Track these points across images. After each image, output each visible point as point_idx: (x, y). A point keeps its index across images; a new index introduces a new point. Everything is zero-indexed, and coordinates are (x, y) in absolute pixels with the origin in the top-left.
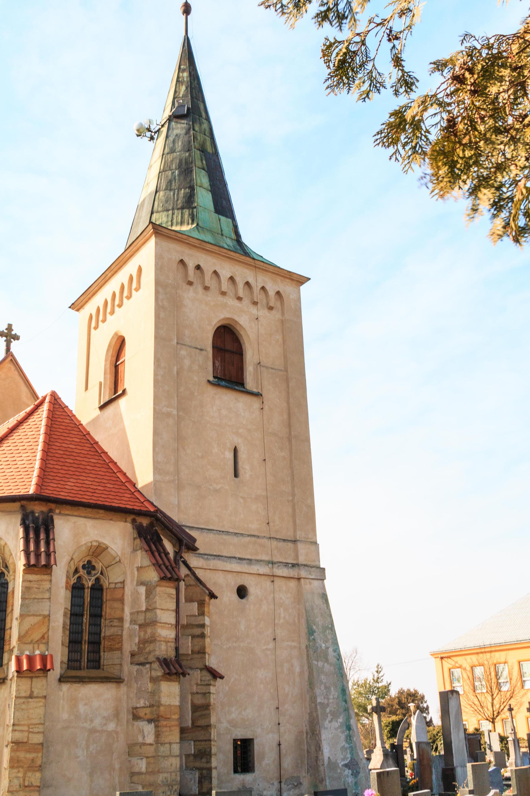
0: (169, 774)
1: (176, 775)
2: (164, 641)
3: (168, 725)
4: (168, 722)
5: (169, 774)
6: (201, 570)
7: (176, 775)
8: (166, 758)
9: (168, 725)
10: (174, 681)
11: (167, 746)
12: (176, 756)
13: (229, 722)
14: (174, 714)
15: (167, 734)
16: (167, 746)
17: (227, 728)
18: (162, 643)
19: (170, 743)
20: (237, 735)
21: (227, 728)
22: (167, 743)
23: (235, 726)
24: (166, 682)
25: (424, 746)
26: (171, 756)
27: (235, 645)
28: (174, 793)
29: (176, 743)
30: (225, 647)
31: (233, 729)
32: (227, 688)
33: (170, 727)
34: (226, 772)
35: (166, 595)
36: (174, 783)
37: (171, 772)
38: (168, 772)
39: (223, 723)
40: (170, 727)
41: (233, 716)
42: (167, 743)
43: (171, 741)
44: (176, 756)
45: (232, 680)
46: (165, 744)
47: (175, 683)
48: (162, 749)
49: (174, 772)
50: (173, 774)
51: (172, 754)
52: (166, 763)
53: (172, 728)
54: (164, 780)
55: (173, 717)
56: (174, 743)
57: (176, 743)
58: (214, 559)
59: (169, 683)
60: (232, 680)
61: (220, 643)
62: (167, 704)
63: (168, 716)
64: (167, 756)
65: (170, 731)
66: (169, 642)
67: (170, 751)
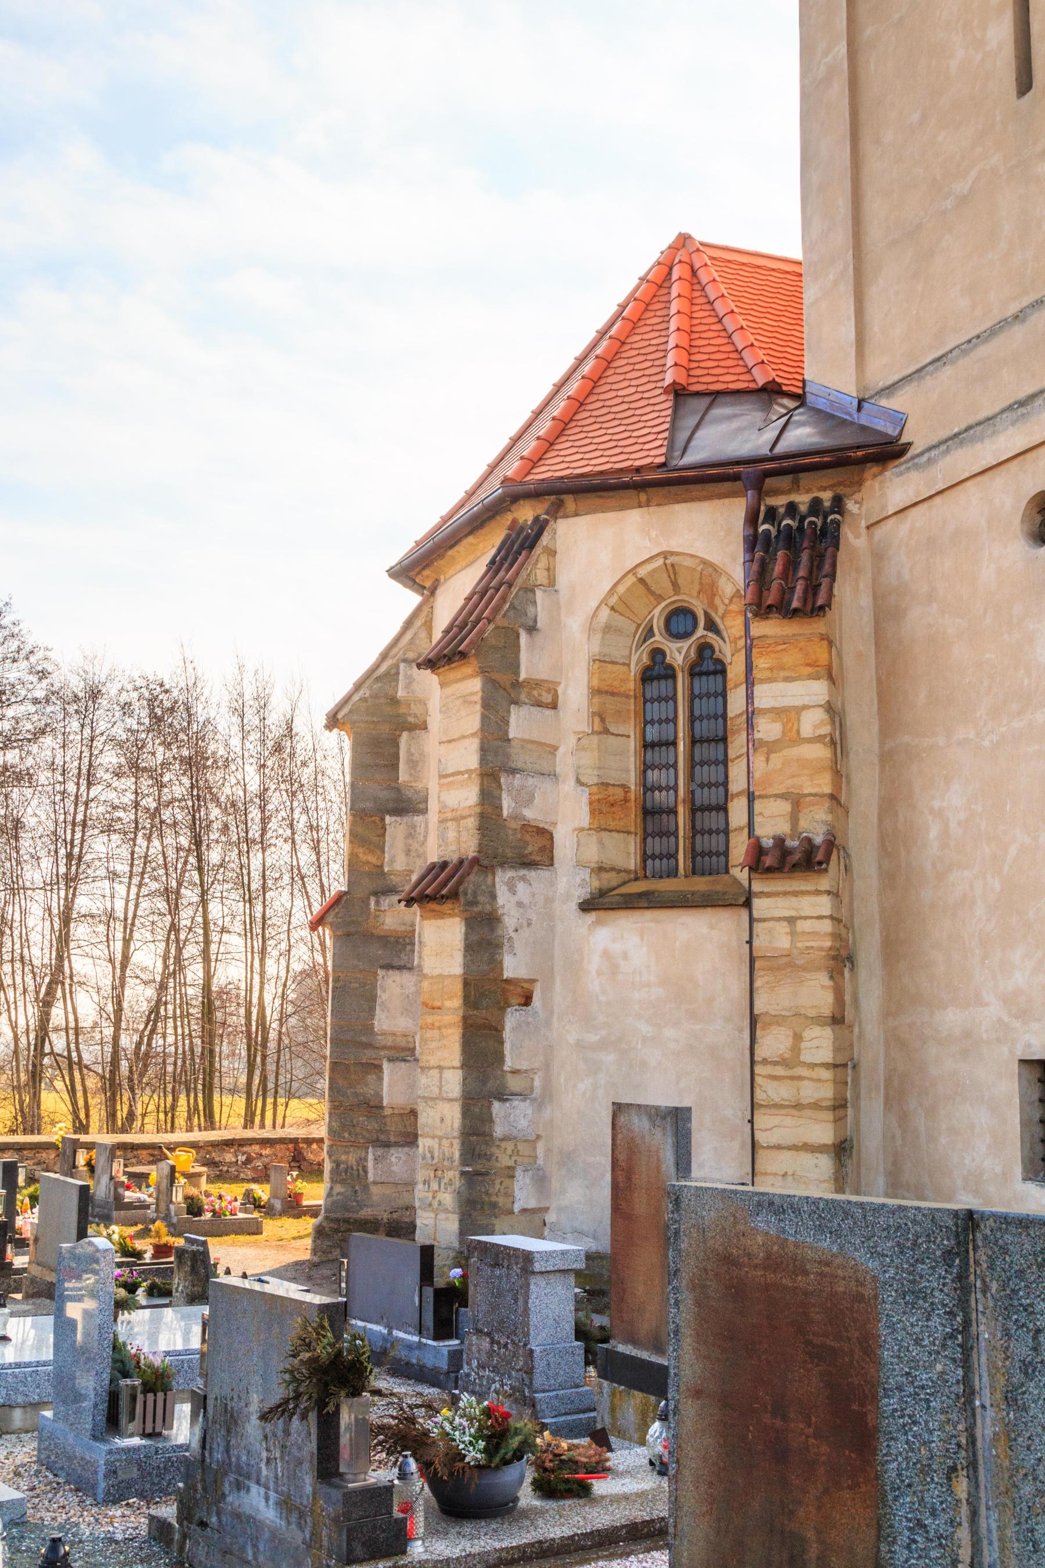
0: (437, 1140)
1: (452, 1145)
2: (451, 820)
3: (437, 1024)
4: (436, 1017)
5: (437, 1140)
6: (915, 510)
7: (452, 1145)
8: (430, 1103)
9: (437, 1024)
10: (451, 916)
11: (434, 1073)
12: (452, 1100)
13: (1008, 1001)
14: (451, 998)
15: (434, 1045)
16: (434, 1073)
17: (1000, 1020)
18: (450, 823)
19: (440, 1068)
20: (1029, 1046)
21: (1000, 1020)
22: (434, 1068)
23: (1024, 1014)
24: (433, 921)
25: (639, 1124)
26: (440, 1098)
27: (1018, 724)
28: (446, 1189)
29: (454, 1068)
30: (986, 743)
31: (1017, 1024)
32: (997, 886)
33: (439, 1028)
34: (998, 1169)
35: (458, 702)
36: (446, 1163)
37: (440, 1138)
38: (433, 1137)
39: (987, 1005)
40: (439, 1028)
41: (1019, 979)
42: (434, 1068)
43: (442, 1064)
44: (452, 1100)
45: (1013, 851)
46: (430, 1068)
47: (452, 920)
48: (423, 1080)
49: (447, 1138)
50: (445, 1142)
51: (445, 1096)
52: (431, 1114)
53: (445, 1032)
54: (428, 1155)
55: (448, 1004)
56: (449, 1068)
57: (454, 1068)
58: (948, 451)
59: (440, 922)
60: (1013, 851)
61: (972, 735)
62: (436, 972)
63: (438, 1004)
64: (436, 1099)
65: (442, 1037)
66: (463, 818)
67: (440, 1087)
